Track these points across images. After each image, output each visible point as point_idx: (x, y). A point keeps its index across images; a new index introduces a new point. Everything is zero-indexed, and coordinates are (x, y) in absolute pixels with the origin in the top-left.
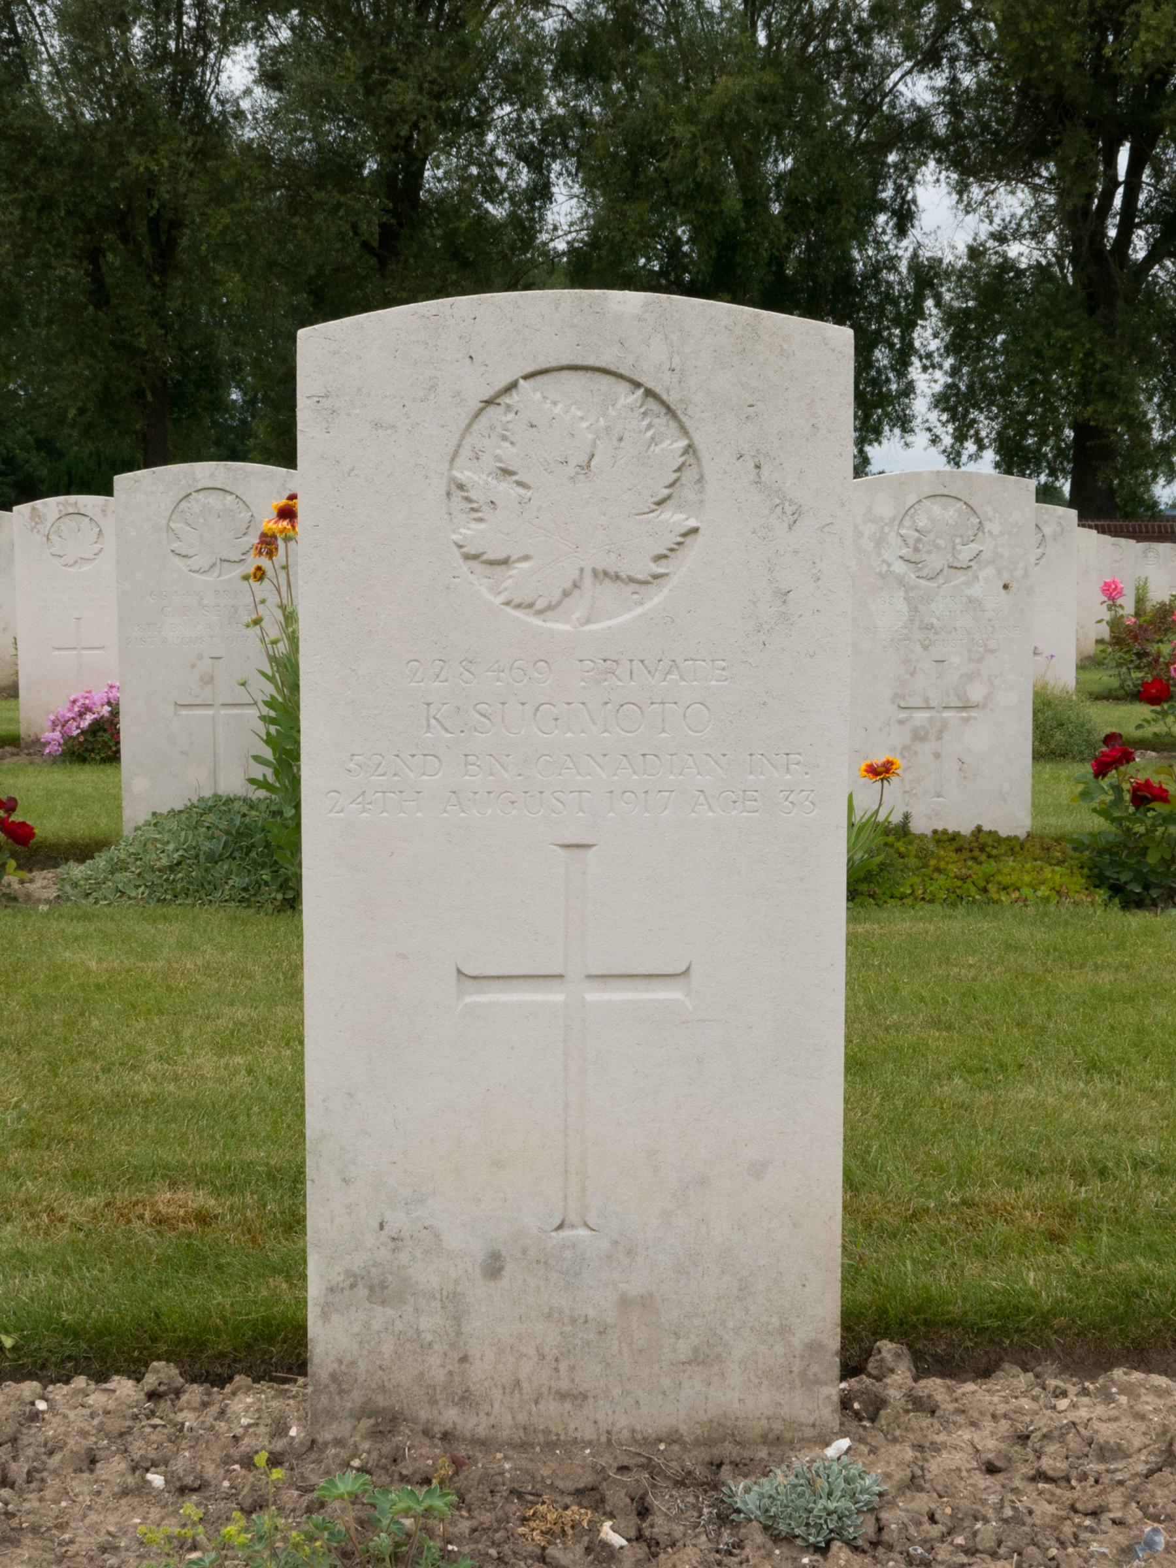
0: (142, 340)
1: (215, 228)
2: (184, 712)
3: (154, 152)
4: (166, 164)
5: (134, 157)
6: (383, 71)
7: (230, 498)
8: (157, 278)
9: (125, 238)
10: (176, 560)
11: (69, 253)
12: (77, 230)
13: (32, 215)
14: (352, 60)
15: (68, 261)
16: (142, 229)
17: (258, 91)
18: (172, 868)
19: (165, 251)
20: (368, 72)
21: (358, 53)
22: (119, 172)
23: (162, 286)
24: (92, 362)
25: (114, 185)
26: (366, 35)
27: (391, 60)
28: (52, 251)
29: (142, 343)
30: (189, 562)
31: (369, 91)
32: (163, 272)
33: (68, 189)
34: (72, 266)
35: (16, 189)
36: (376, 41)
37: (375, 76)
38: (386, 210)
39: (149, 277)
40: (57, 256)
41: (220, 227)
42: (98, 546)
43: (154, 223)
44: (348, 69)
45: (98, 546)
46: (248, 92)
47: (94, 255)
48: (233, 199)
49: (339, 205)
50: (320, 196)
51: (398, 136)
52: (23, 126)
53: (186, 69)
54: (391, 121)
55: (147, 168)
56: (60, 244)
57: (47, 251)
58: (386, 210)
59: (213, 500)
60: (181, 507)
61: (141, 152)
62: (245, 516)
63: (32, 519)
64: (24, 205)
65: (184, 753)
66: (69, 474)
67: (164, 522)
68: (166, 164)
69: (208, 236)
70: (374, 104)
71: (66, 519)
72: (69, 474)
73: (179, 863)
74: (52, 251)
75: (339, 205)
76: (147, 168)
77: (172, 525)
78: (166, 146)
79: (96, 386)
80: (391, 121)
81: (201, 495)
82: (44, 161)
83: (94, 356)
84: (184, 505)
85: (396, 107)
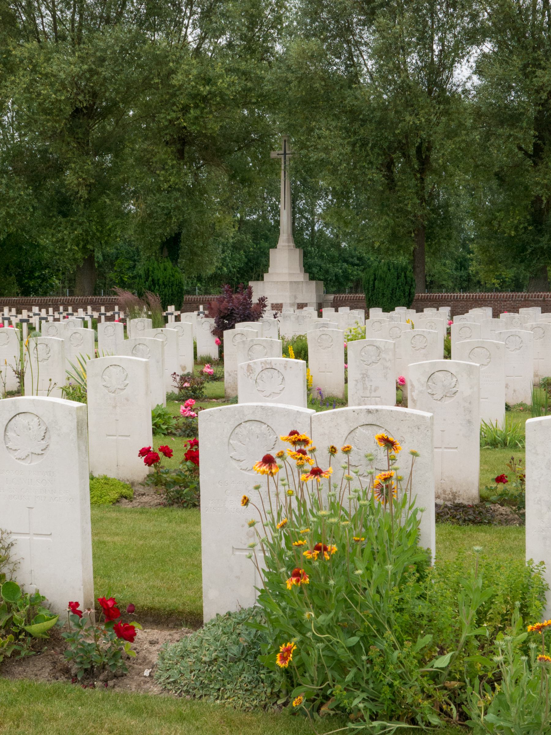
0: (409, 206)
1: (446, 151)
2: (237, 553)
3: (416, 115)
4: (423, 120)
5: (408, 118)
6: (534, 65)
7: (264, 426)
8: (419, 175)
9: (404, 155)
10: (234, 463)
11: (374, 167)
12: (378, 154)
13: (357, 149)
14: (517, 61)
15: (373, 171)
16: (413, 151)
17: (475, 78)
18: (211, 663)
19: (425, 163)
20: (526, 66)
21: (520, 57)
22: (400, 125)
23: (422, 180)
24: (388, 219)
25: (397, 132)
26: (524, 48)
27: (539, 60)
28: (366, 166)
29: (409, 208)
30: (241, 464)
31: (526, 76)
32: (422, 171)
33: (374, 133)
34: (376, 173)
35: (350, 137)
36: (530, 50)
37: (529, 69)
38: (535, 137)
39: (415, 175)
40: (369, 169)
41: (449, 150)
42: (282, 386)
43: (419, 150)
44: (514, 66)
45: (282, 386)
46: (469, 78)
47: (389, 166)
48: (456, 135)
49: (510, 135)
50: (500, 131)
51: (541, 98)
52: (353, 105)
53: (436, 72)
54: (537, 92)
55: (414, 122)
56: (371, 163)
57: (364, 167)
58: (535, 137)
59: (255, 427)
60: (236, 431)
61: (411, 115)
62: (273, 437)
63: (248, 371)
64: (354, 145)
65: (237, 577)
66: (375, 274)
67: (226, 440)
68: (423, 120)
69: (443, 154)
70: (528, 83)
71: (266, 371)
72: (375, 274)
73: (215, 660)
74: (366, 166)
75: (510, 135)
76: (414, 122)
77: (231, 441)
78: (423, 111)
79: (389, 231)
80: (537, 92)
81: (248, 424)
82: (364, 121)
83: (388, 215)
84: (238, 430)
85: (541, 84)
